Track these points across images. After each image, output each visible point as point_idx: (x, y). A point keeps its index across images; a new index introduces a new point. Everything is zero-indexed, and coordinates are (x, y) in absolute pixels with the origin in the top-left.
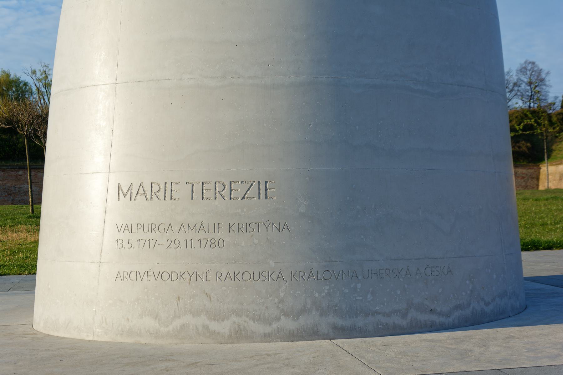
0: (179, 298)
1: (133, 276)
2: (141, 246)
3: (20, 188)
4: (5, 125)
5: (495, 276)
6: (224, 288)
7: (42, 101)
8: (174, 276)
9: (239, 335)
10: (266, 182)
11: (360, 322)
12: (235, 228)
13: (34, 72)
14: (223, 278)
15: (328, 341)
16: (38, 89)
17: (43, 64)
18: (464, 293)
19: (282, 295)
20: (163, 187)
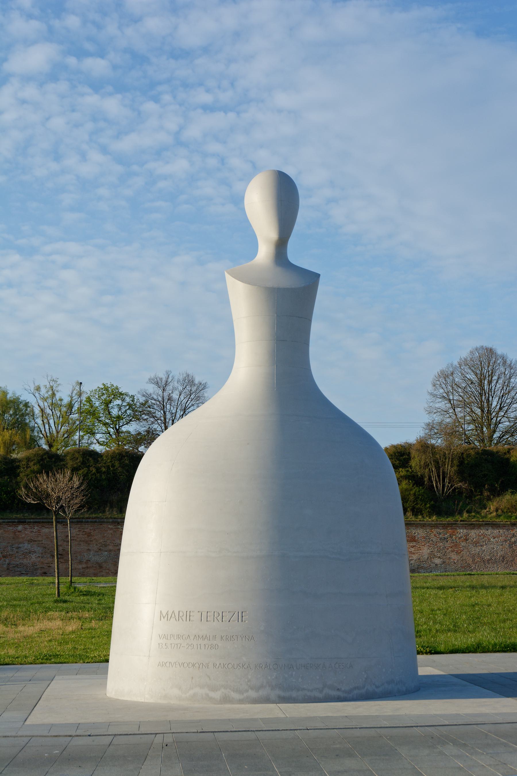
0: (192, 678)
1: (168, 664)
2: (172, 647)
3: (18, 548)
4: (33, 500)
5: (384, 670)
6: (217, 673)
7: (47, 426)
8: (190, 665)
9: (225, 700)
10: (242, 612)
11: (294, 694)
12: (224, 638)
13: (38, 389)
14: (217, 667)
15: (275, 705)
16: (42, 411)
17: (49, 378)
18: (361, 680)
19: (250, 677)
20: (185, 614)
